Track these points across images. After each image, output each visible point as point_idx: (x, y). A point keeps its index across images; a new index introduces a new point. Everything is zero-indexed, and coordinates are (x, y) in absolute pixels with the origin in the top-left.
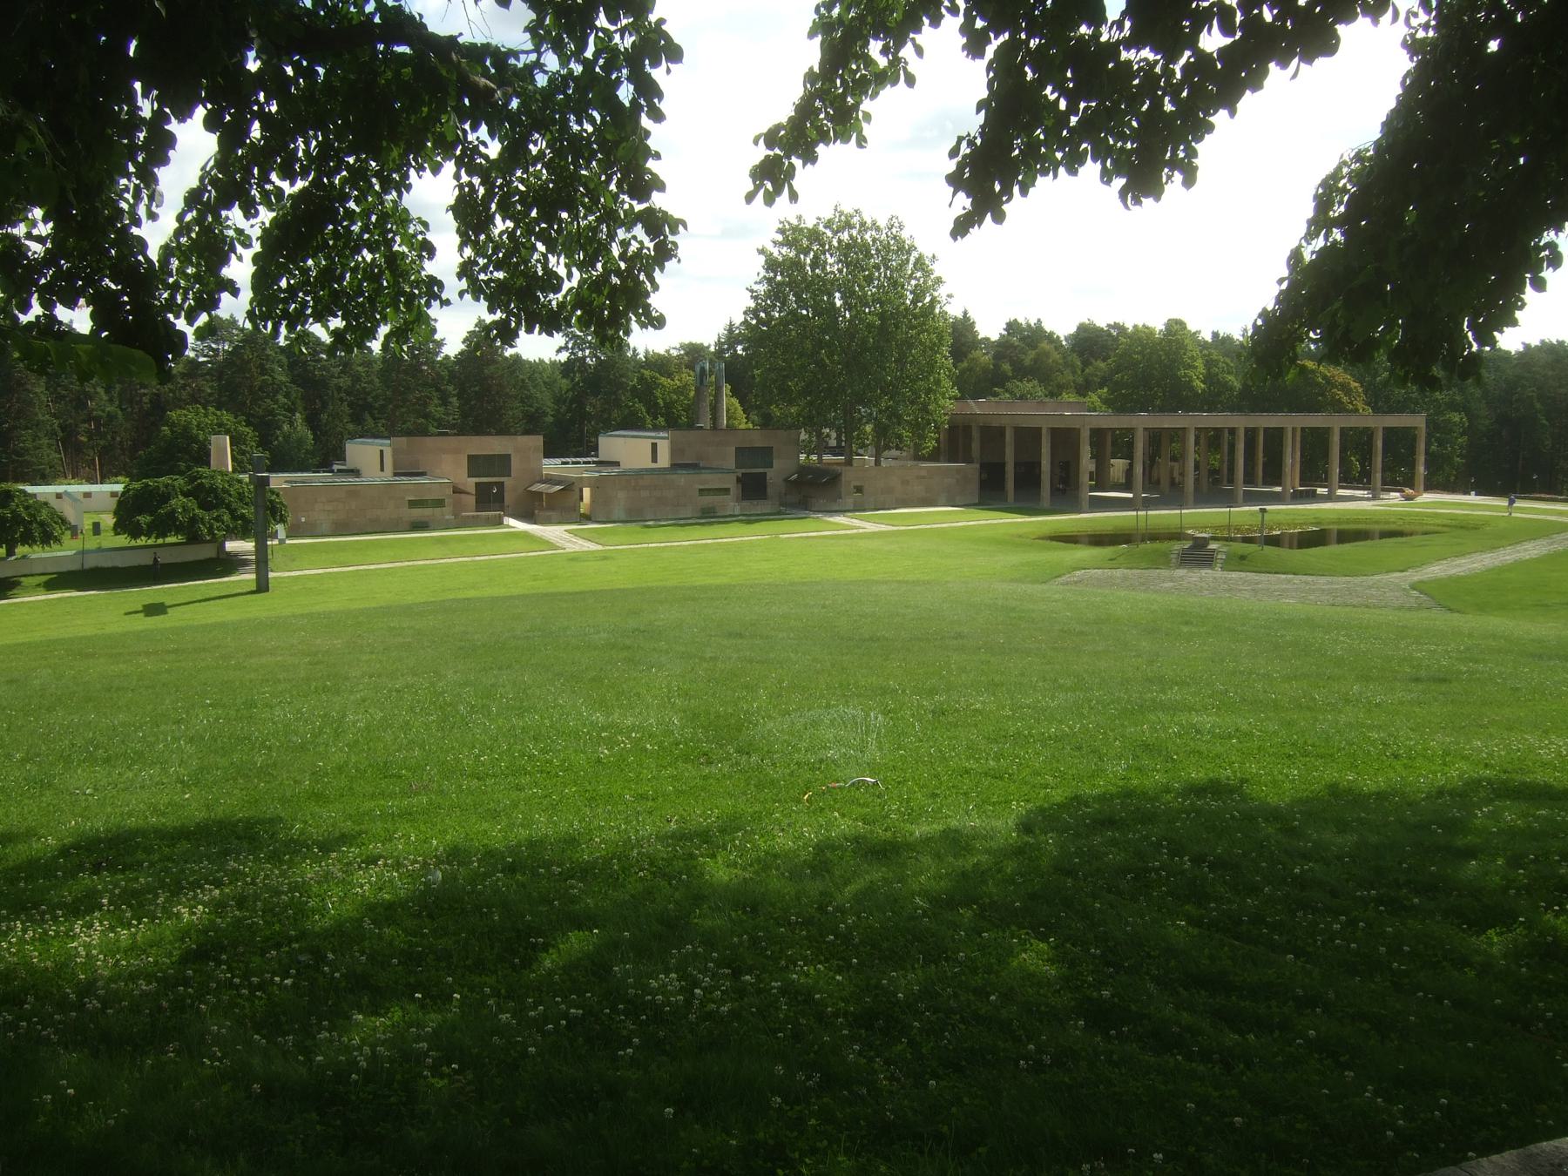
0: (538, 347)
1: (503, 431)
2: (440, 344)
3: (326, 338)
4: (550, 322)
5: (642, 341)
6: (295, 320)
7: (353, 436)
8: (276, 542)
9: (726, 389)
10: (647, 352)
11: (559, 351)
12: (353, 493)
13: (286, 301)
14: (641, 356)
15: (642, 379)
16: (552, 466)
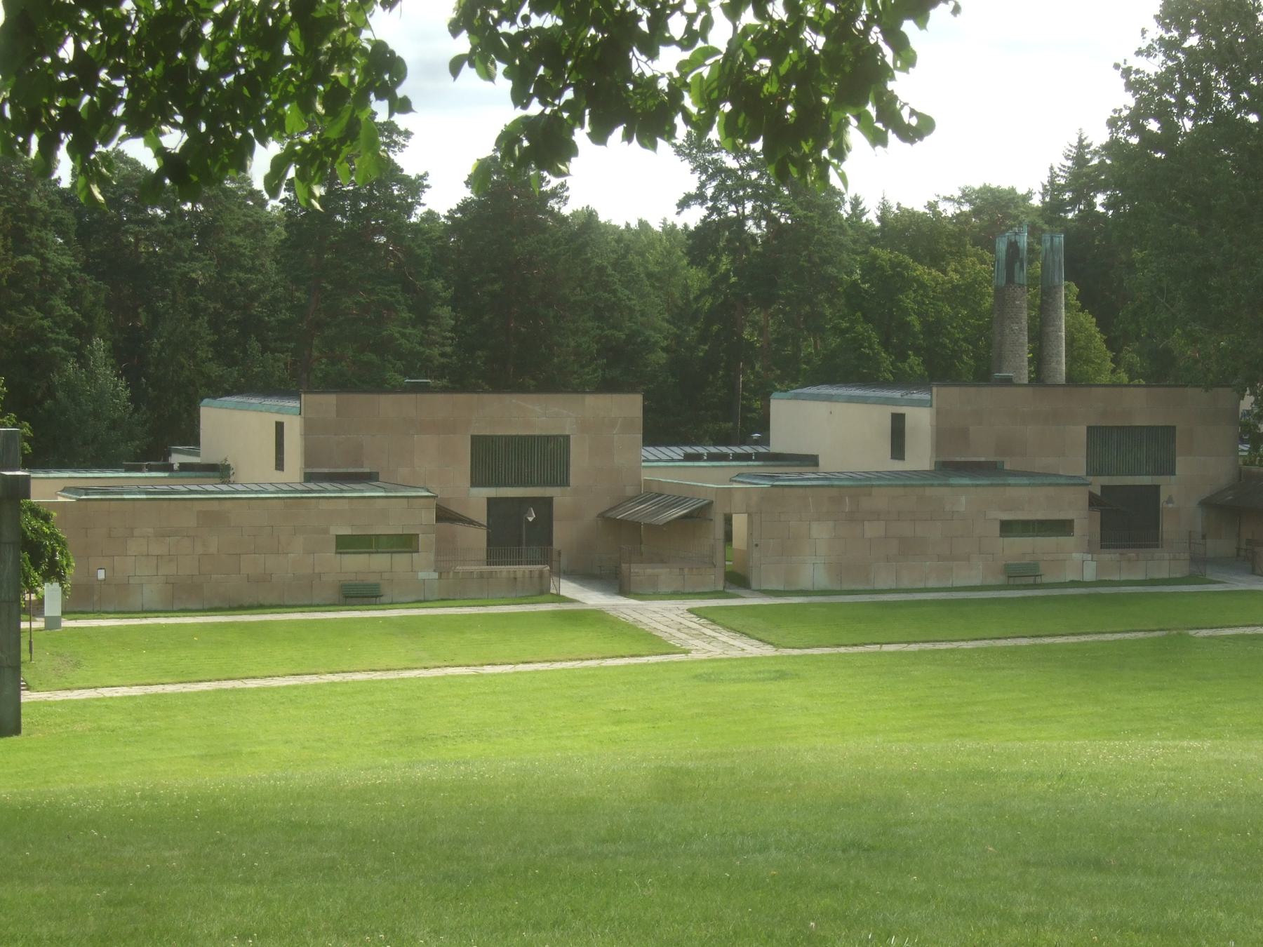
0: (628, 185)
1: (551, 382)
2: (416, 186)
3: (151, 163)
4: (648, 117)
5: (876, 178)
6: (88, 132)
7: (219, 390)
8: (39, 624)
9: (1066, 292)
10: (885, 209)
11: (684, 203)
12: (212, 518)
13: (70, 90)
14: (872, 217)
15: (871, 268)
16: (665, 467)
